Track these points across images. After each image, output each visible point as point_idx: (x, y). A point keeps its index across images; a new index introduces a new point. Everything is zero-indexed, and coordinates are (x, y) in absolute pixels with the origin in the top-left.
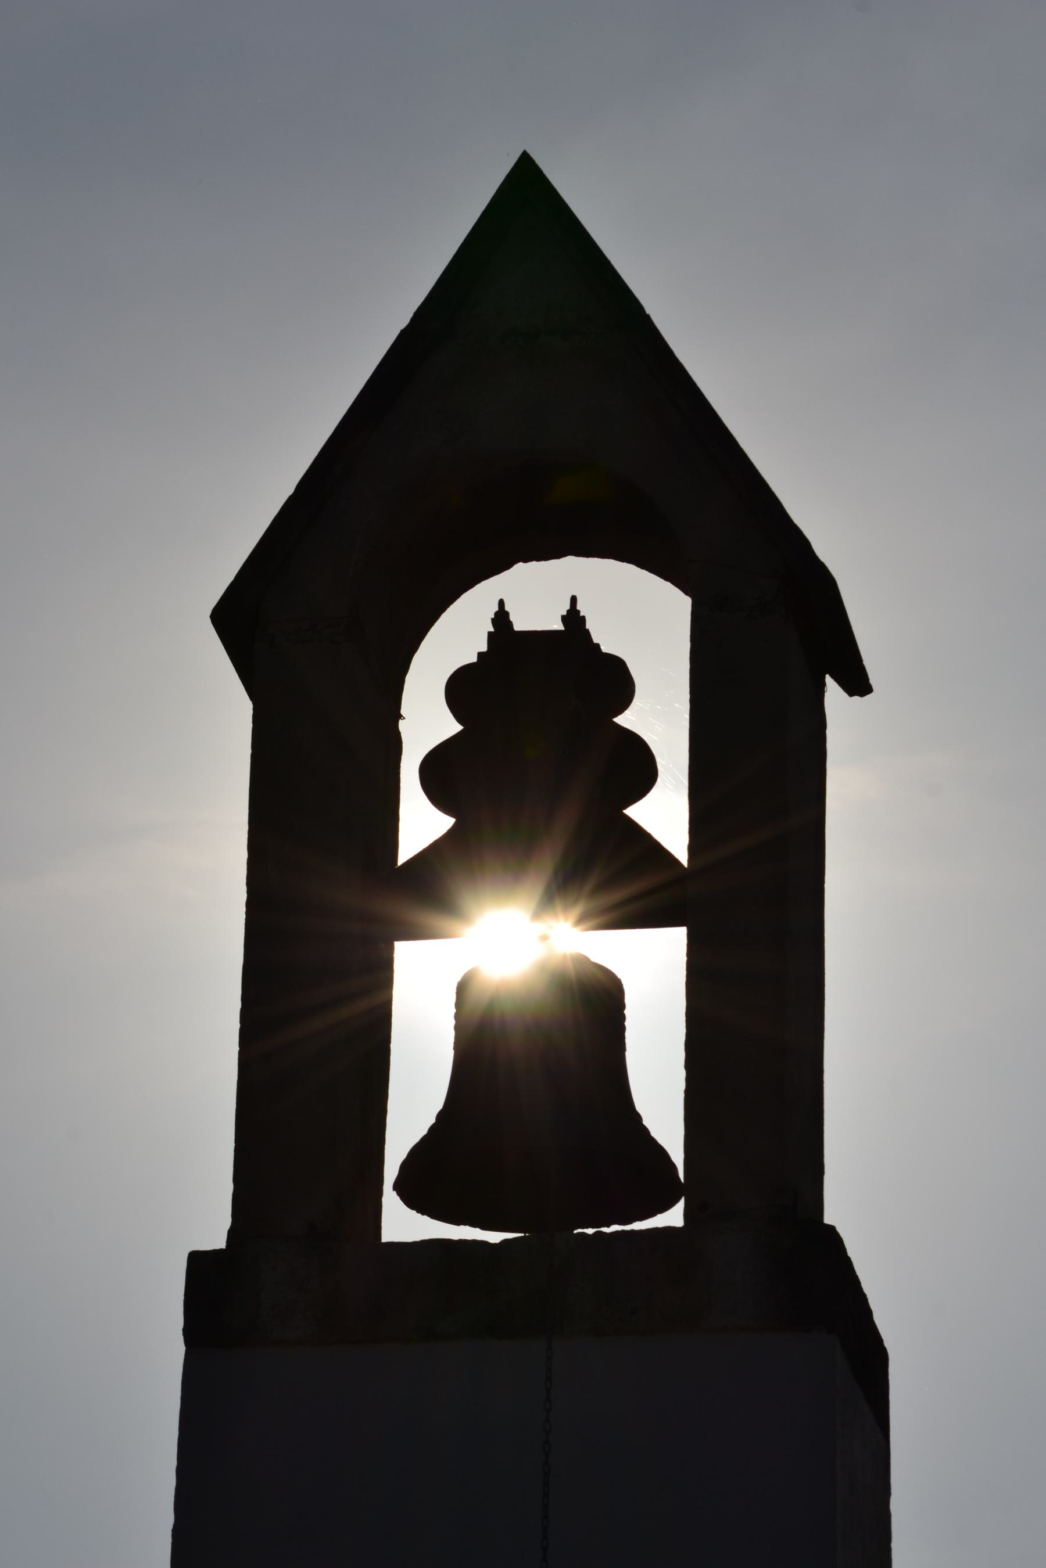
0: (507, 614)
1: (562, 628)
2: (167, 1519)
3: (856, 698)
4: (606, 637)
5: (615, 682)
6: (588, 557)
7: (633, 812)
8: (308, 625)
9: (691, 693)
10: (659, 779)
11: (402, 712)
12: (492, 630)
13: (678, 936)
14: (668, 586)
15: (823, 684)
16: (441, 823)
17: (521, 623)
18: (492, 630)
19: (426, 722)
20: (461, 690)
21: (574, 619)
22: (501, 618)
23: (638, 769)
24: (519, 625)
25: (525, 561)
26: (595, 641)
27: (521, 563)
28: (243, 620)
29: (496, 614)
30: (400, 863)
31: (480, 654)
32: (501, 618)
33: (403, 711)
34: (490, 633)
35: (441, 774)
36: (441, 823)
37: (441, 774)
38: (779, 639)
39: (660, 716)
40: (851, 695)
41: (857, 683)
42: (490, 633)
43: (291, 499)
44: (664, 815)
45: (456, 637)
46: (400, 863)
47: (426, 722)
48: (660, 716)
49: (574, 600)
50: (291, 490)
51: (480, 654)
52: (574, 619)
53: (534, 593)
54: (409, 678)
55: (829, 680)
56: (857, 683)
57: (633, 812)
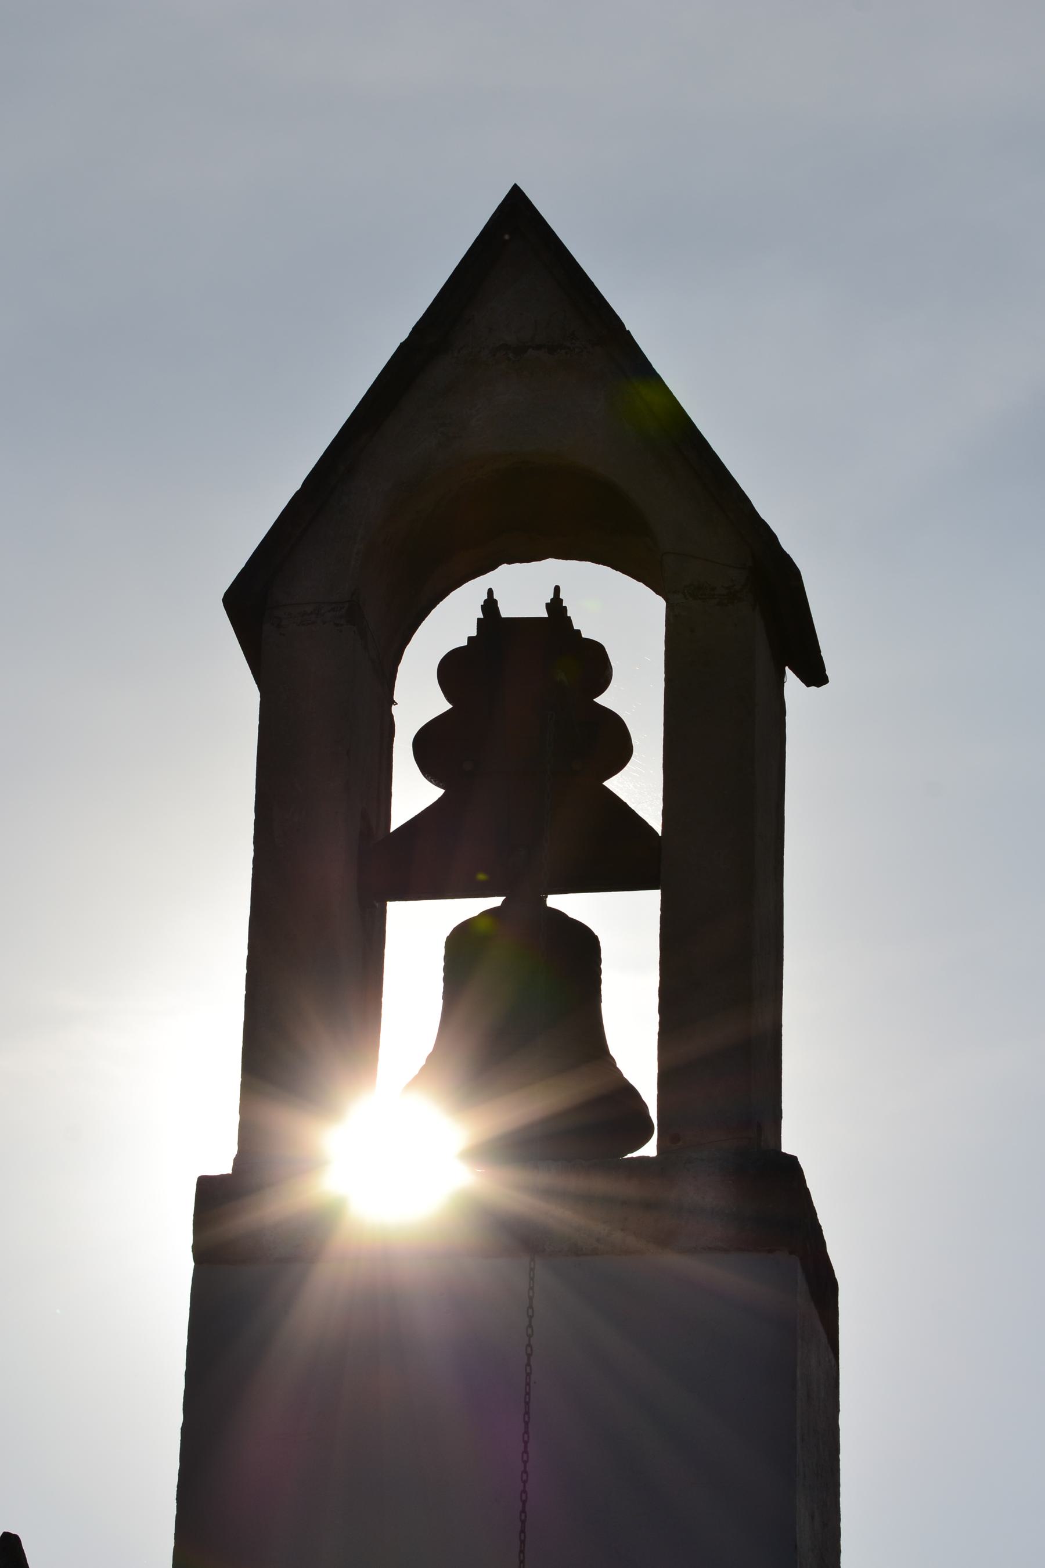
0: (496, 601)
1: (546, 615)
2: (177, 1418)
3: (813, 688)
4: (586, 622)
5: (594, 664)
6: (567, 559)
7: (612, 784)
8: (309, 608)
9: (666, 673)
10: (634, 753)
11: (395, 698)
12: (482, 616)
13: (659, 891)
14: (641, 586)
15: (784, 672)
16: (431, 793)
17: (507, 611)
18: (482, 616)
19: (418, 698)
20: (452, 670)
21: (556, 606)
22: (490, 605)
23: (616, 746)
24: (505, 613)
25: (509, 563)
26: (576, 627)
27: (505, 565)
28: (253, 604)
29: (485, 601)
30: (394, 826)
31: (470, 639)
32: (490, 605)
33: (396, 697)
34: (479, 619)
35: (429, 747)
36: (431, 793)
37: (429, 747)
38: (751, 630)
39: (637, 695)
40: (808, 685)
41: (814, 674)
42: (479, 619)
43: (298, 494)
44: (640, 787)
45: (450, 623)
46: (394, 826)
47: (418, 698)
48: (637, 695)
49: (557, 589)
50: (298, 487)
51: (470, 639)
52: (556, 606)
53: (522, 588)
54: (401, 668)
55: (787, 668)
56: (814, 674)
57: (612, 784)
